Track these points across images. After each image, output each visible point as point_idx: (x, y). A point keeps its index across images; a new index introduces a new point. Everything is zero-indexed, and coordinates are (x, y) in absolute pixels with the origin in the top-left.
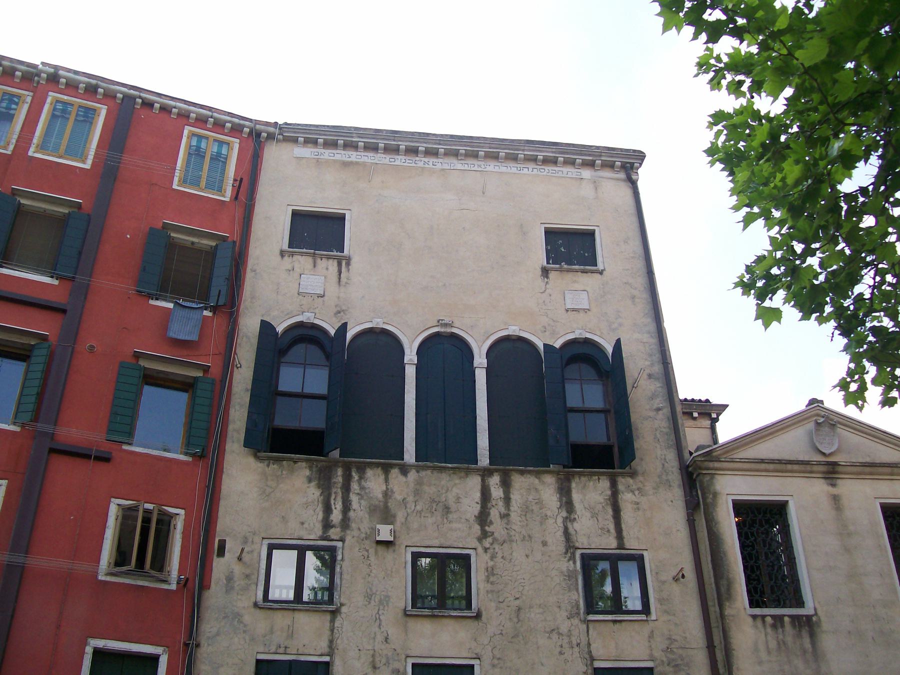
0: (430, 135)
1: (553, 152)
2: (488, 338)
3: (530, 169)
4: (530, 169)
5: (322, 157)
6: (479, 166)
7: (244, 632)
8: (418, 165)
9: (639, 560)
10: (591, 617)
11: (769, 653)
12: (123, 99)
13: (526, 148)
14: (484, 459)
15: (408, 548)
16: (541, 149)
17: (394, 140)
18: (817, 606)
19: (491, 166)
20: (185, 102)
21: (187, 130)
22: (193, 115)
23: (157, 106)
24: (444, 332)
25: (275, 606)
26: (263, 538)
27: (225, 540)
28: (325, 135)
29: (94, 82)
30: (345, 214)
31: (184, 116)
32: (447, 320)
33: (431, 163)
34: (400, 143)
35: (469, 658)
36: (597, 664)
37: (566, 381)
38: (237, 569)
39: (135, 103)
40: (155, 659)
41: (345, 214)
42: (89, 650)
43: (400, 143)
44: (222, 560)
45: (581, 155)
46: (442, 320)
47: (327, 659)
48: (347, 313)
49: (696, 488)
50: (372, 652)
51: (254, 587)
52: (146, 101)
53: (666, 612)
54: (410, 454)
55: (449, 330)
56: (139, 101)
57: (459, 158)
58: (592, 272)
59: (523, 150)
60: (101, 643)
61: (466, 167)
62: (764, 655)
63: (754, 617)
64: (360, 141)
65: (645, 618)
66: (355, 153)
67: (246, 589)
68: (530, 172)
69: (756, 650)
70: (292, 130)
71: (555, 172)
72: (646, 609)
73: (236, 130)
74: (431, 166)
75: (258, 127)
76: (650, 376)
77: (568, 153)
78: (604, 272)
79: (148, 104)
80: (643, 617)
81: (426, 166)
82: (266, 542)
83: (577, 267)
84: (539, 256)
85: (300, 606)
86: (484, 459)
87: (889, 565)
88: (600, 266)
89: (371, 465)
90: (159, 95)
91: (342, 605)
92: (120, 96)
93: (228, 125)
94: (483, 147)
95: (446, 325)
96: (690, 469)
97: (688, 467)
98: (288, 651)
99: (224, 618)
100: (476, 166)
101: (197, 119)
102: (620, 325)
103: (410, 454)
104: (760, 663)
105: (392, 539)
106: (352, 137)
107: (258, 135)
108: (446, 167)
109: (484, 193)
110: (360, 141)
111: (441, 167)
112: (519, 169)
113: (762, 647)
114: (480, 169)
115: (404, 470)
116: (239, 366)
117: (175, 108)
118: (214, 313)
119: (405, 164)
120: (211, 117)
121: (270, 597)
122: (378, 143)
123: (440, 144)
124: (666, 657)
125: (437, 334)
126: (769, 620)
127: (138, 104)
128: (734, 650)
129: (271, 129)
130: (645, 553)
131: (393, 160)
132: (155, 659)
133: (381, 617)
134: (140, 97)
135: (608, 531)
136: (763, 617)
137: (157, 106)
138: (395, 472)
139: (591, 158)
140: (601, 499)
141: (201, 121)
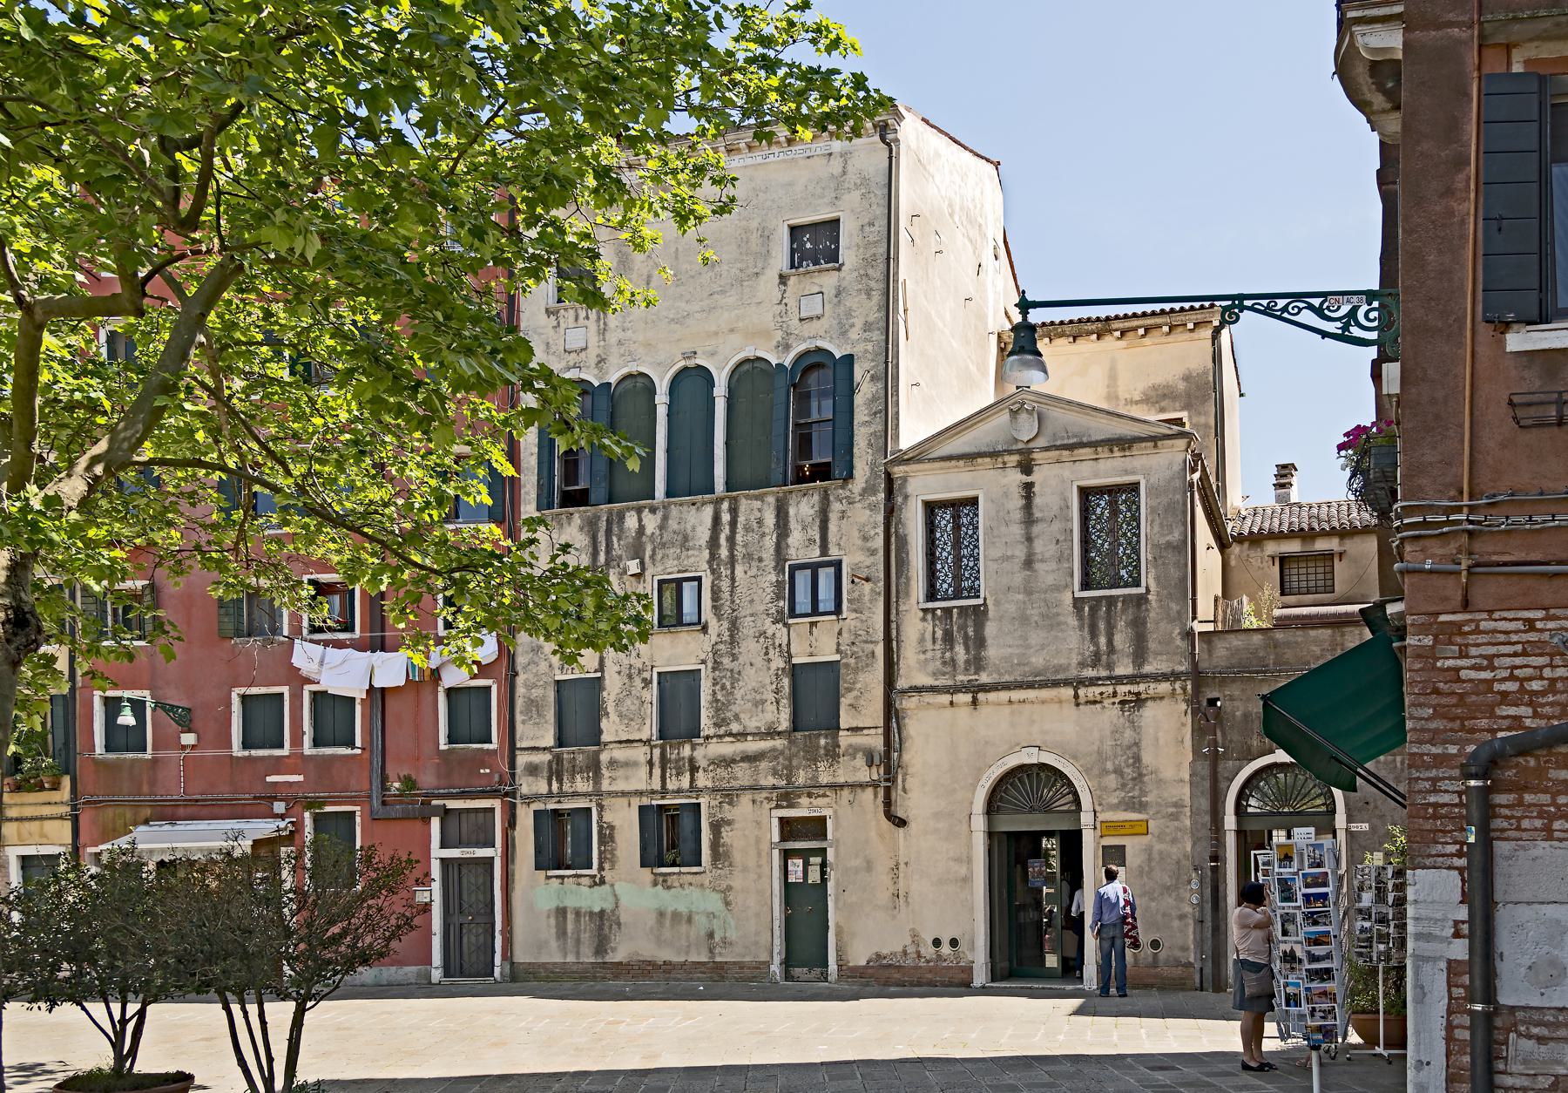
9: (838, 565)
11: (934, 642)
18: (988, 596)
35: (951, 138)
36: (795, 661)
37: (518, 752)
47: (599, 675)
53: (855, 611)
62: (929, 645)
63: (925, 611)
64: (1499, 656)
69: (922, 640)
72: (838, 610)
76: (873, 378)
84: (780, 257)
87: (1417, 1033)
89: (628, 509)
102: (852, 326)
110: (1499, 656)
113: (928, 636)
125: (686, 369)
126: (939, 612)
132: (488, 688)
136: (934, 610)
140: (812, 512)
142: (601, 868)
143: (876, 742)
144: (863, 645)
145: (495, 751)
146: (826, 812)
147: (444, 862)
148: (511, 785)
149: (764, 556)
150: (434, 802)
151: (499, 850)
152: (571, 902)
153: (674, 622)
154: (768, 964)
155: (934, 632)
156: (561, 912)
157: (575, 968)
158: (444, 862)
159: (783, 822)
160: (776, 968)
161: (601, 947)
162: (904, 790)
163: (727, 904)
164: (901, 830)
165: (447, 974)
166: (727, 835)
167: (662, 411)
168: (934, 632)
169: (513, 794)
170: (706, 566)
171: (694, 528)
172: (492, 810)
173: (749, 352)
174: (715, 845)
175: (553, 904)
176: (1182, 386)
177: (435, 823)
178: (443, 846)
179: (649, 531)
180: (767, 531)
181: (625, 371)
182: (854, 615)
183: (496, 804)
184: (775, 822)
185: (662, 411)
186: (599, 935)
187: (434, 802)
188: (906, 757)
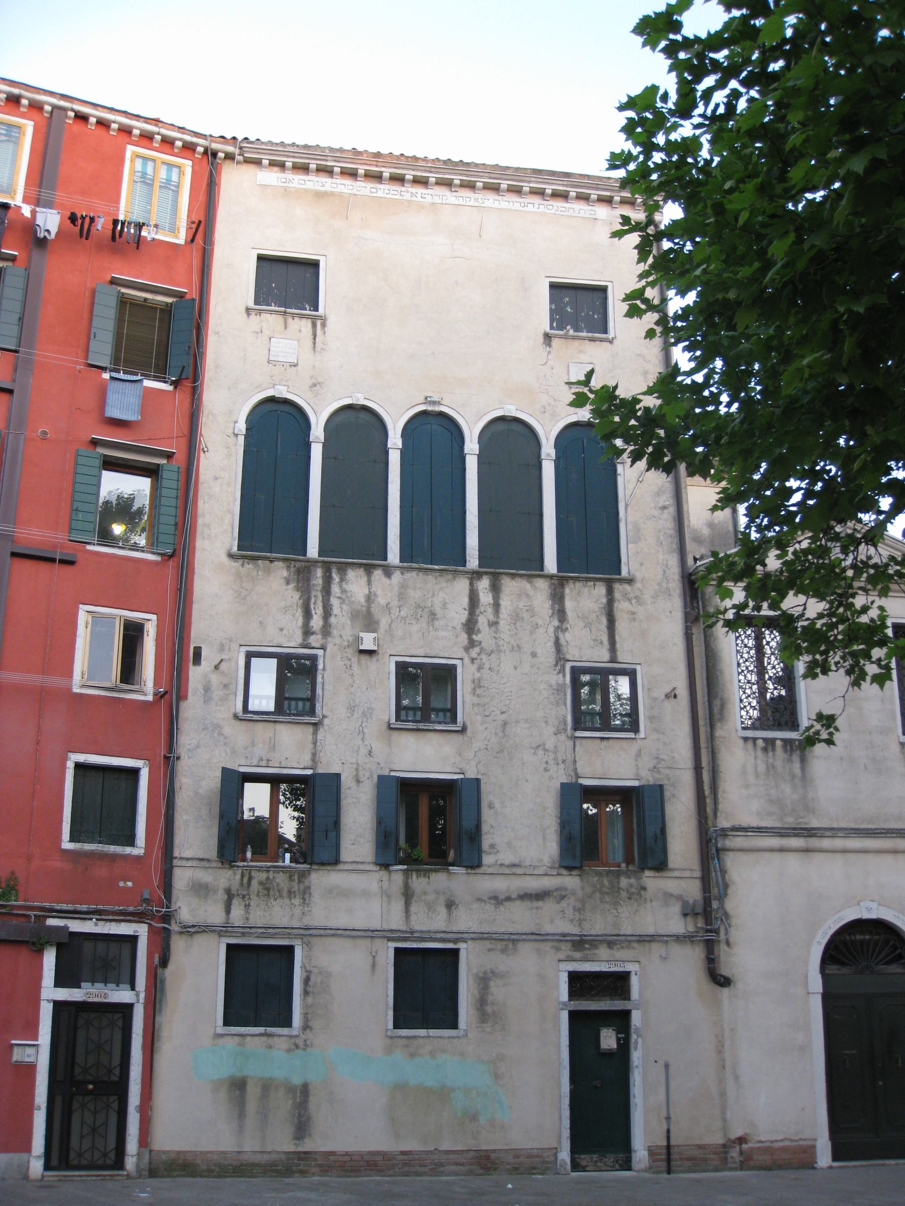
0: (420, 161)
1: (563, 185)
2: (481, 418)
3: (536, 206)
4: (536, 206)
5: (291, 185)
6: (476, 200)
7: (225, 744)
8: (405, 198)
9: (632, 674)
10: (579, 734)
12: (52, 113)
13: (532, 179)
14: (473, 561)
15: (392, 657)
16: (549, 181)
17: (377, 166)
19: (490, 200)
20: (125, 113)
21: (130, 149)
22: (136, 132)
23: (93, 120)
24: (432, 411)
25: (256, 717)
26: (241, 645)
27: (200, 648)
28: (294, 157)
29: (16, 91)
30: (319, 261)
31: (126, 131)
32: (436, 398)
33: (419, 195)
34: (383, 169)
37: (175, 862)
38: (215, 679)
39: (67, 117)
40: (134, 773)
41: (319, 261)
42: (70, 765)
43: (383, 169)
44: (197, 668)
45: (597, 189)
46: (430, 397)
48: (323, 385)
49: (698, 598)
50: (355, 766)
51: (232, 697)
52: (79, 114)
54: (394, 555)
55: (437, 408)
56: (72, 114)
57: (453, 190)
58: (602, 340)
59: (529, 182)
60: (82, 758)
61: (461, 201)
62: (751, 778)
63: (746, 739)
65: (633, 736)
66: (329, 180)
67: (224, 699)
68: (535, 209)
69: (744, 772)
70: (280, 153)
71: (396, 193)
73: (189, 148)
74: (419, 199)
75: (215, 146)
77: (581, 187)
78: (615, 341)
79: (82, 118)
80: (632, 735)
81: (414, 199)
82: (244, 649)
83: (584, 334)
85: (281, 718)
86: (473, 561)
88: (611, 335)
90: (95, 106)
91: (324, 717)
92: (48, 108)
93: (136, 132)
94: (482, 177)
95: (434, 403)
96: (693, 578)
97: (690, 575)
98: (271, 764)
99: (204, 729)
100: (473, 199)
101: (141, 135)
103: (394, 555)
104: (747, 786)
105: (375, 648)
106: (327, 160)
107: (214, 154)
108: (437, 200)
109: (480, 236)
111: (431, 201)
112: (523, 205)
113: (750, 769)
114: (476, 204)
115: (388, 571)
116: (206, 449)
117: (114, 122)
118: (175, 388)
119: (389, 196)
120: (158, 134)
121: (251, 708)
122: (357, 169)
123: (431, 172)
124: (652, 776)
125: (424, 413)
126: (760, 743)
127: (69, 118)
128: (721, 772)
129: (230, 149)
130: (638, 668)
131: (375, 190)
132: (134, 773)
133: (364, 730)
134: (73, 110)
135: (601, 643)
136: (755, 740)
137: (93, 120)
138: (378, 574)
139: (608, 194)
141: (147, 137)
142: (306, 1027)
143: (693, 890)
144: (667, 771)
145: (138, 858)
146: (629, 967)
147: (59, 1006)
148: (168, 907)
149: (539, 651)
150: (51, 922)
151: (142, 996)
152: (254, 1070)
153: (308, 704)
154: (556, 1151)
155: (756, 766)
156: (238, 1085)
157: (258, 1158)
158: (59, 1006)
159: (574, 977)
160: (565, 1155)
161: (302, 1128)
162: (728, 943)
163: (497, 1076)
164: (725, 991)
165: (47, 1167)
166: (497, 991)
167: (395, 458)
168: (756, 766)
169: (167, 918)
170: (461, 653)
171: (444, 606)
172: (133, 940)
173: (511, 410)
174: (482, 1002)
175: (226, 1070)
176: (677, 203)
177: (49, 959)
178: (59, 982)
179: (381, 601)
180: (540, 622)
181: (348, 401)
182: (654, 736)
183: (141, 930)
184: (564, 978)
185: (395, 458)
186: (300, 1116)
187: (51, 922)
188: (729, 905)
